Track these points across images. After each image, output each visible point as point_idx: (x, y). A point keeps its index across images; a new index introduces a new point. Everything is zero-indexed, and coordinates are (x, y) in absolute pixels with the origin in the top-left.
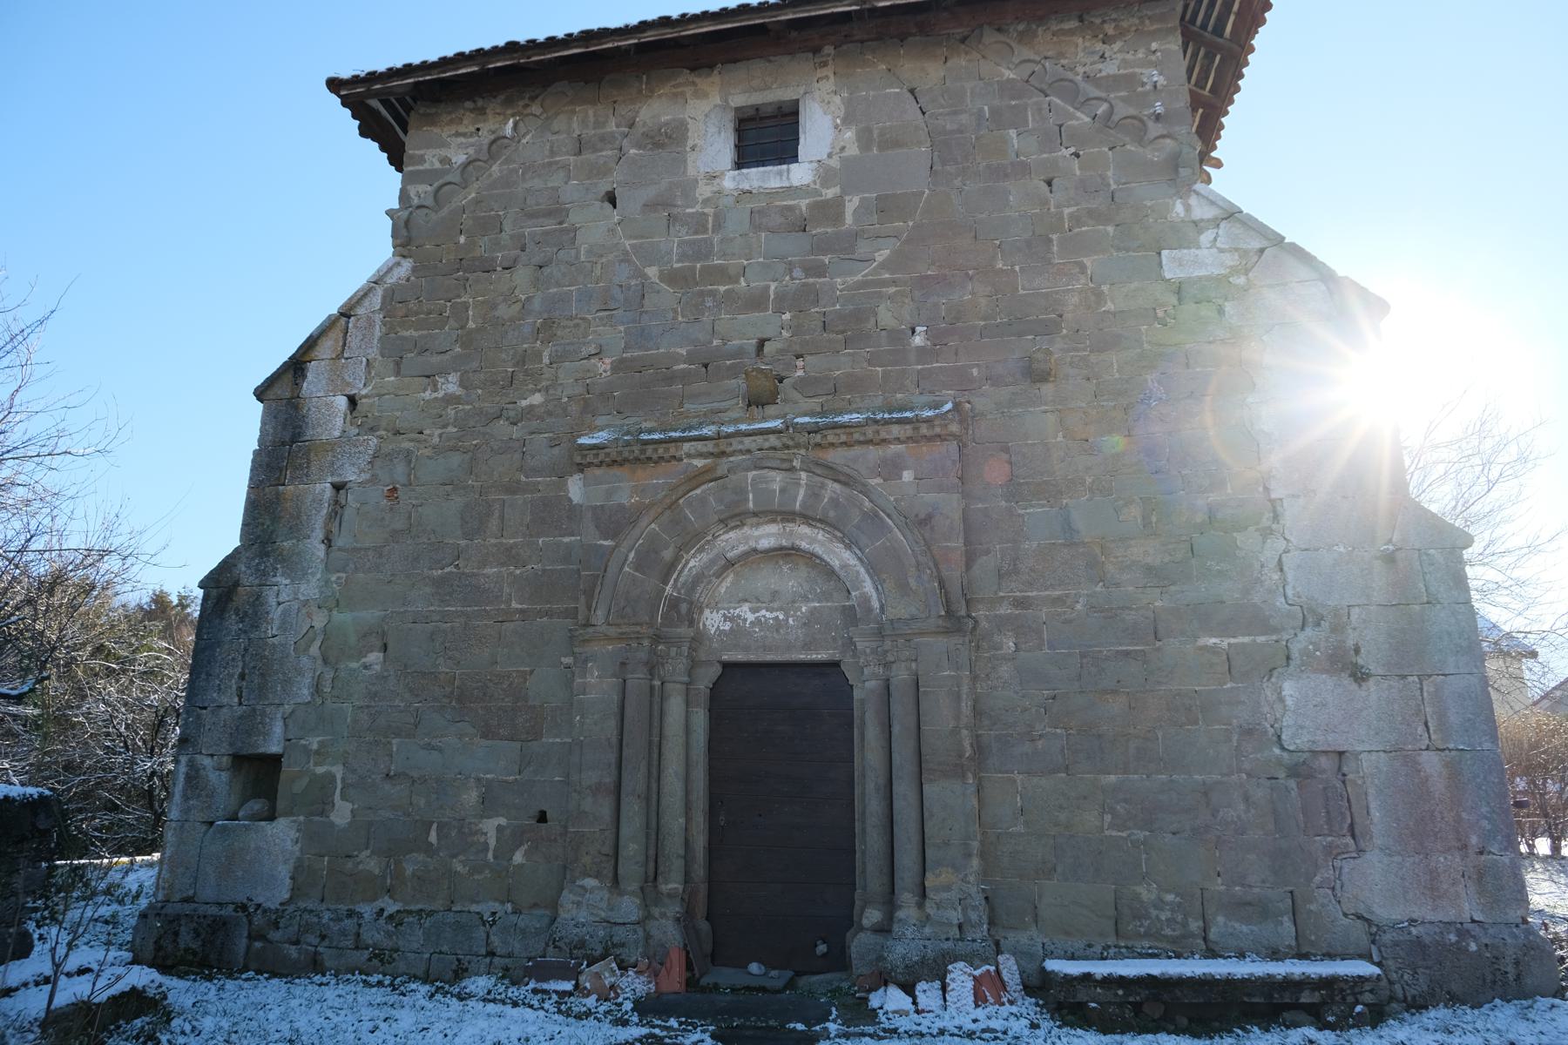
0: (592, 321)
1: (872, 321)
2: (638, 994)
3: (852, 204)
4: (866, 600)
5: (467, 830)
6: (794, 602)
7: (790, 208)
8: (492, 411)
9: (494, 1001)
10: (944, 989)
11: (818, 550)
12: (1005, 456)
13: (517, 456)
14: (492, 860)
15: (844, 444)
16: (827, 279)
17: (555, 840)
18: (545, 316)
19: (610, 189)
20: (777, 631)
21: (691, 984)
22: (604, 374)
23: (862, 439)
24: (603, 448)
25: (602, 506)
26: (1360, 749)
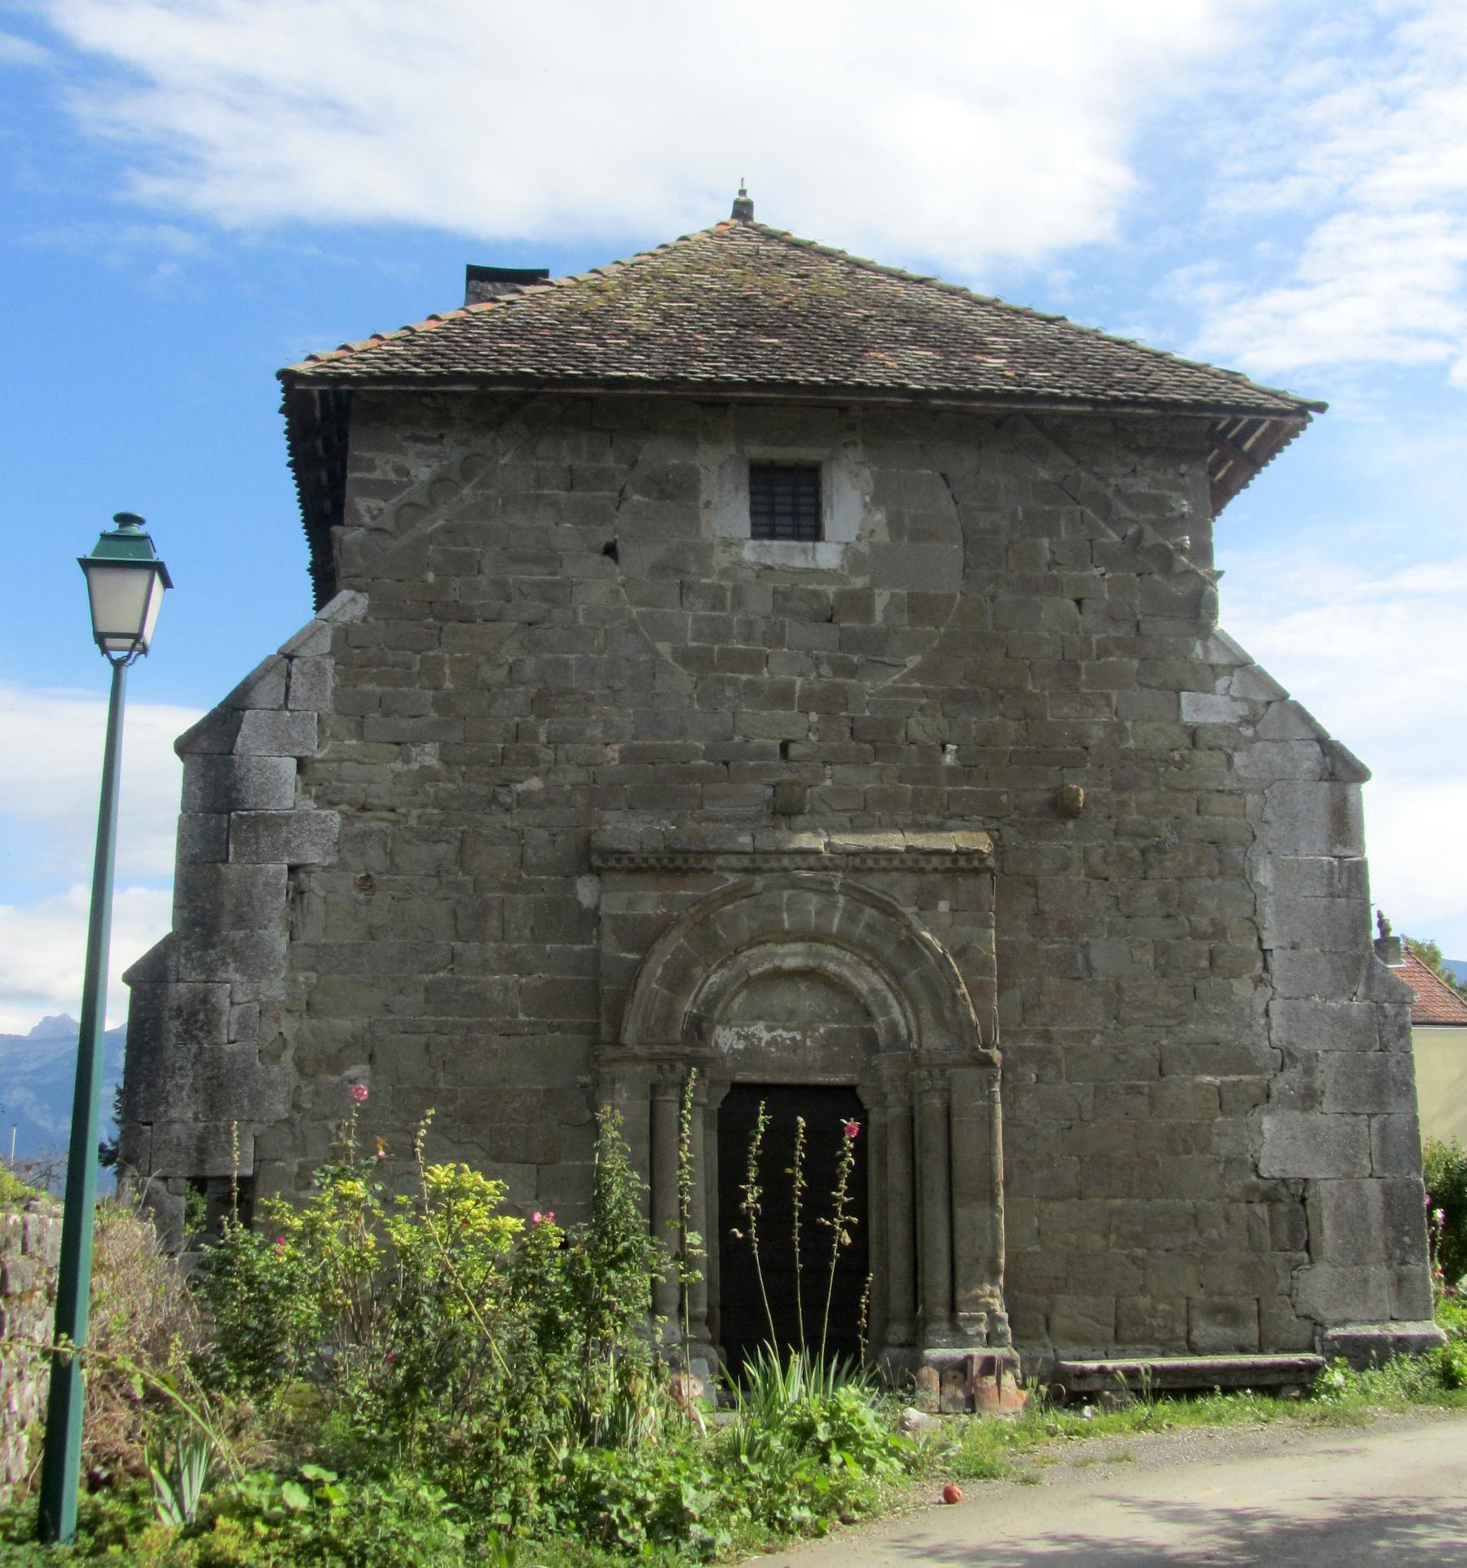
1: (903, 733)
3: (881, 599)
4: (892, 1026)
6: (811, 1022)
7: (816, 594)
11: (847, 973)
12: (1031, 891)
19: (611, 540)
20: (795, 1051)
26: (1319, 1176)
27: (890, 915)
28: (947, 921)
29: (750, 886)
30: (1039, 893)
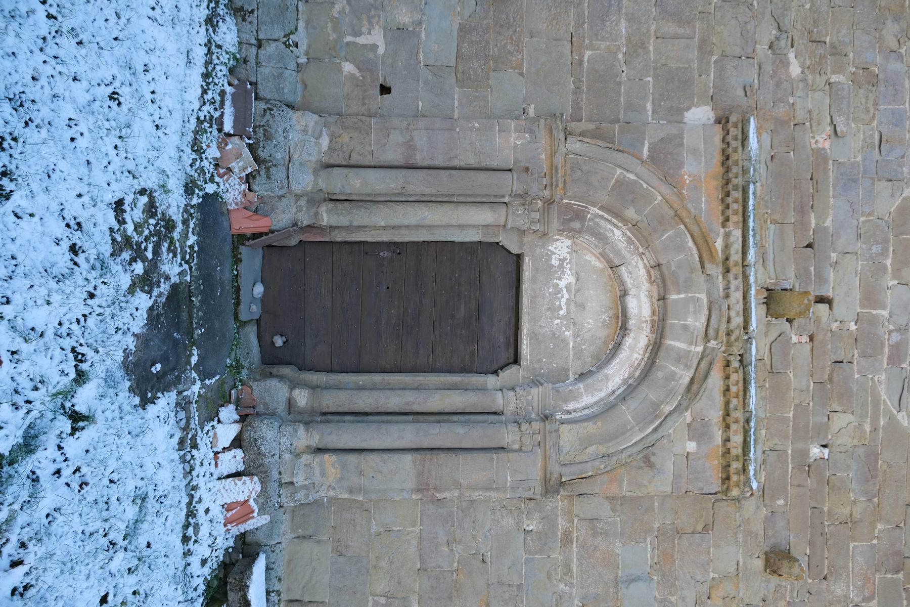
0: (870, 127)
2: (224, 196)
4: (575, 397)
5: (373, 13)
6: (574, 324)
8: (786, 22)
9: (210, 52)
10: (237, 475)
11: (623, 354)
12: (700, 528)
13: (738, 51)
14: (345, 41)
15: (727, 389)
16: (885, 366)
17: (364, 104)
18: (881, 76)
20: (549, 309)
21: (241, 239)
22: (813, 141)
23: (731, 406)
24: (743, 146)
25: (682, 145)
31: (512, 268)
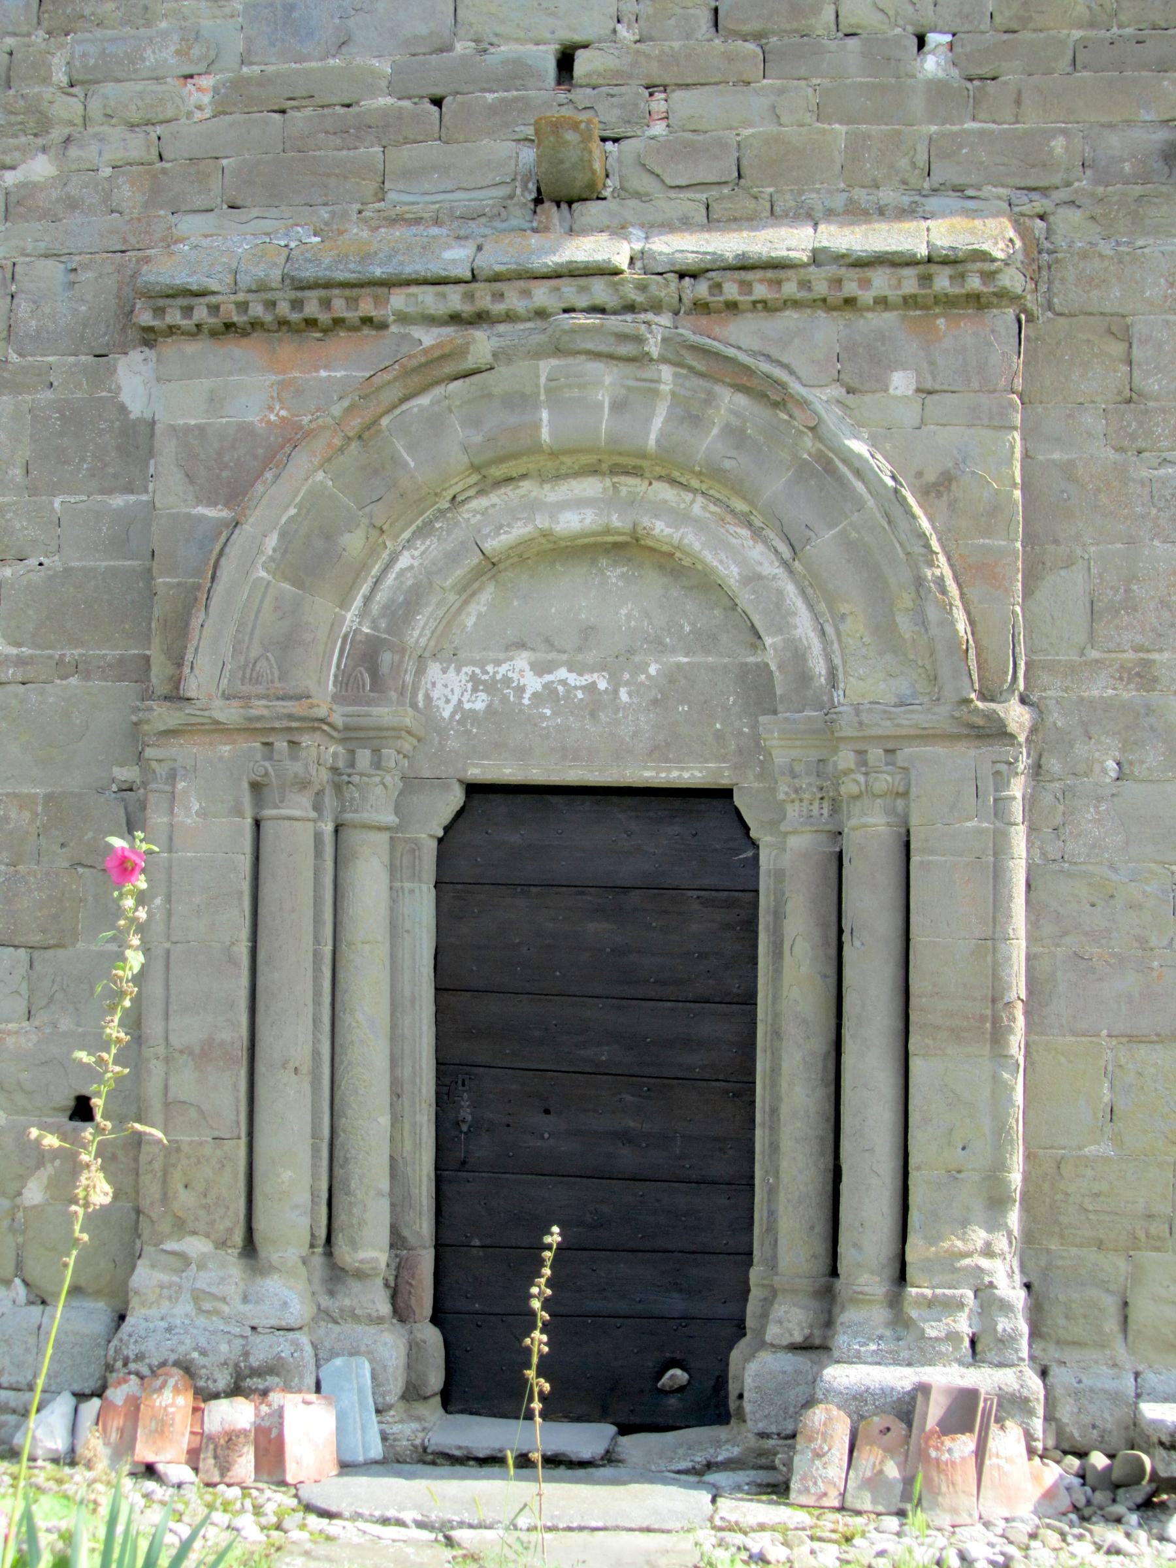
4: (797, 656)
6: (631, 651)
11: (692, 540)
12: (1117, 348)
20: (593, 715)
23: (802, 295)
25: (201, 429)
27: (776, 405)
28: (910, 414)
29: (460, 352)
30: (1136, 353)
31: (500, 806)
